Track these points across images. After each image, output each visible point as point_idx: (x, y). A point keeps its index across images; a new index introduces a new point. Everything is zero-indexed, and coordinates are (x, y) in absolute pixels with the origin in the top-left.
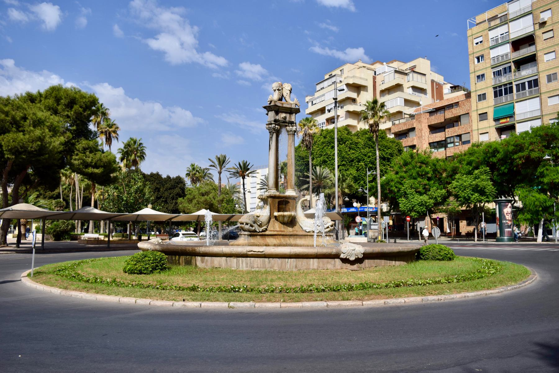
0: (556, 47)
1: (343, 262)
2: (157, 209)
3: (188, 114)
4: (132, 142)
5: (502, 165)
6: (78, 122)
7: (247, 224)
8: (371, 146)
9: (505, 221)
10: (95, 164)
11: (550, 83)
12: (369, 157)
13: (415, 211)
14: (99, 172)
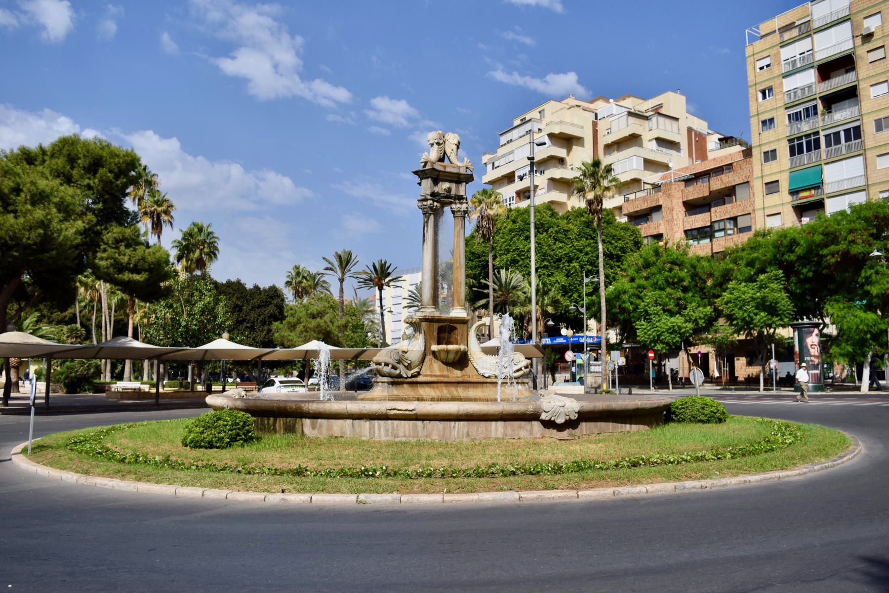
1: (545, 427)
2: (236, 342)
3: (287, 182)
4: (196, 230)
5: (804, 266)
6: (106, 197)
7: (387, 364)
8: (590, 235)
10: (135, 265)
11: (880, 133)
12: (587, 254)
13: (662, 342)
14: (142, 279)
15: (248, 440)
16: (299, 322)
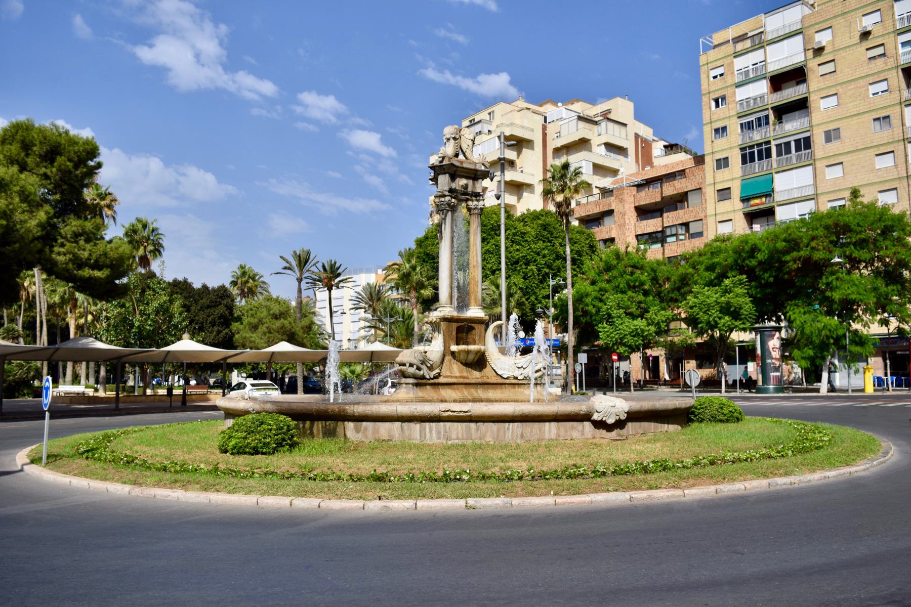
0: (839, 87)
1: (595, 427)
2: (180, 341)
3: (210, 178)
4: (140, 226)
5: (765, 271)
6: (65, 187)
7: (411, 365)
8: (548, 238)
9: (770, 361)
10: (96, 261)
11: (829, 144)
12: (544, 256)
13: (624, 345)
14: (103, 276)
15: (293, 445)
16: (261, 322)
